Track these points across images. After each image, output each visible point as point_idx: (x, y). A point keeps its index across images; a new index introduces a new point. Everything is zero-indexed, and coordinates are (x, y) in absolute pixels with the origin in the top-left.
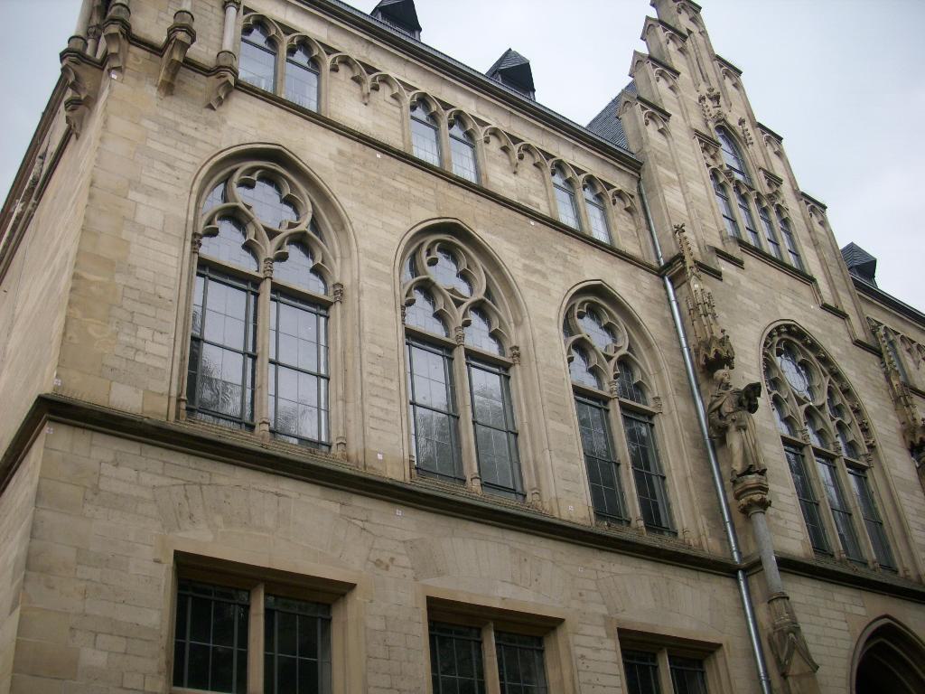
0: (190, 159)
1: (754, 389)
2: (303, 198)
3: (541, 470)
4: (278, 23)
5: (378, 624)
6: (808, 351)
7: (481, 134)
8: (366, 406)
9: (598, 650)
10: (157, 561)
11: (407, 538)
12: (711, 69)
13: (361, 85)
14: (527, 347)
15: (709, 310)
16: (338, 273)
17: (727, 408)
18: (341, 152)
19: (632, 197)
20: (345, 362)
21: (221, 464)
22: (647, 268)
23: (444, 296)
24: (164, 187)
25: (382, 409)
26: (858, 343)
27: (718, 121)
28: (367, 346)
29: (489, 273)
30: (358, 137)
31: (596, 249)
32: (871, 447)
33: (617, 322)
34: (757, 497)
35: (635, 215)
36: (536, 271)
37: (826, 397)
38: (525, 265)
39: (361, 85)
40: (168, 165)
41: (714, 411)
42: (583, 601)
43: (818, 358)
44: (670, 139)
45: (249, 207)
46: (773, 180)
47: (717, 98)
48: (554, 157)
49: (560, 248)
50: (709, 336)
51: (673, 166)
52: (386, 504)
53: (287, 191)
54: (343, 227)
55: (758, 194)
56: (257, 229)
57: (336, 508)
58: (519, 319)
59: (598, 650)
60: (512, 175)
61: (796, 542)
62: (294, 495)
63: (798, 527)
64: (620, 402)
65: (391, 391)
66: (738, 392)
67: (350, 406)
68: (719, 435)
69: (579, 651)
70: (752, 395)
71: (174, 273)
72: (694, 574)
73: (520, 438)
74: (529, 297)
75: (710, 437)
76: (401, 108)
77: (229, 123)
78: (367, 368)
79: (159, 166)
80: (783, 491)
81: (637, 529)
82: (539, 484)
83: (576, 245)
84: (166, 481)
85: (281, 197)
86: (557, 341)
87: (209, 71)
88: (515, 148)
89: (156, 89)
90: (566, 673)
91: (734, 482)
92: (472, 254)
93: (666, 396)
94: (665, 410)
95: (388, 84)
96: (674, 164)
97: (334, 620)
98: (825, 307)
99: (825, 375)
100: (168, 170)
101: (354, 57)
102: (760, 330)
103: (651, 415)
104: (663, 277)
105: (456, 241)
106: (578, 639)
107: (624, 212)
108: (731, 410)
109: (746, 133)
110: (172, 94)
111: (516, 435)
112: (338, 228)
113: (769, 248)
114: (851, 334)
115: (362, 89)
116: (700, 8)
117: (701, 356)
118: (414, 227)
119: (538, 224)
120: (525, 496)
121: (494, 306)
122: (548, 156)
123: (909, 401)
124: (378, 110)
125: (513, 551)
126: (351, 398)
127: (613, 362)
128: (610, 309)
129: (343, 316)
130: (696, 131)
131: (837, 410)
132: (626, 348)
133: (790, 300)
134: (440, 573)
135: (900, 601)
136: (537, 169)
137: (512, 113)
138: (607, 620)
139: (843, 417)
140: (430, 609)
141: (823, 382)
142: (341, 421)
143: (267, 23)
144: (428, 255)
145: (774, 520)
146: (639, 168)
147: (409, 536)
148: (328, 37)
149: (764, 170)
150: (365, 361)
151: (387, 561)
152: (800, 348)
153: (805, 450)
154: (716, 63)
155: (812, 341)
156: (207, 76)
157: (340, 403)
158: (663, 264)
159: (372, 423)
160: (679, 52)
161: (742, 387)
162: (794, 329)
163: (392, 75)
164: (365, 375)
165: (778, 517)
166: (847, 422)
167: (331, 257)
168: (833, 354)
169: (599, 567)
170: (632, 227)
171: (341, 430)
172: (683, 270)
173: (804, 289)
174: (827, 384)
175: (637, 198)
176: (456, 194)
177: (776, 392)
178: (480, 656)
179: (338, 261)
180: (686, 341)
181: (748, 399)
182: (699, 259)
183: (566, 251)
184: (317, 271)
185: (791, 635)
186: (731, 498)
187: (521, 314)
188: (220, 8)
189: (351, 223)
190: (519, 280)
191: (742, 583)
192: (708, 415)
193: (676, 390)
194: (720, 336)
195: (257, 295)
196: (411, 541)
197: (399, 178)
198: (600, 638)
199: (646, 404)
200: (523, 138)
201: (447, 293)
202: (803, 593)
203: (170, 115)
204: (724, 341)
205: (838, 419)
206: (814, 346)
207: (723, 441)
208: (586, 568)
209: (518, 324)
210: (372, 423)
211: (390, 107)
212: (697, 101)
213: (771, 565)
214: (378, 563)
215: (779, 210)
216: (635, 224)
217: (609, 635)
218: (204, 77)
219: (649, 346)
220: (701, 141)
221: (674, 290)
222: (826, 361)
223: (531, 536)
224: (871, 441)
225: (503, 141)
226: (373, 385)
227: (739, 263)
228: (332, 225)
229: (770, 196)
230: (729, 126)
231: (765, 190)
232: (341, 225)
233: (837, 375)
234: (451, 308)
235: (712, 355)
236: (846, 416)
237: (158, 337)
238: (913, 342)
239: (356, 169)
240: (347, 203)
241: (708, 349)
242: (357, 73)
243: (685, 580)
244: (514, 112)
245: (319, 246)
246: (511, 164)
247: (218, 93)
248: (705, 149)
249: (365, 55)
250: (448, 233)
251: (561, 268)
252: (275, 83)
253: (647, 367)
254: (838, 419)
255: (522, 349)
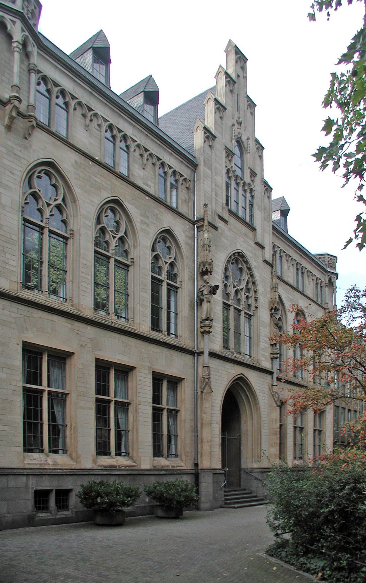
0: (20, 169)
1: (217, 287)
2: (60, 185)
3: (135, 311)
4: (52, 80)
5: (81, 366)
6: (244, 263)
7: (133, 147)
8: (80, 286)
9: (145, 378)
10: (18, 344)
11: (91, 337)
12: (243, 104)
13: (85, 119)
14: (137, 259)
15: (208, 249)
16: (71, 225)
17: (205, 292)
18: (76, 162)
19: (190, 181)
20: (73, 266)
21: (35, 309)
22: (189, 220)
23: (109, 233)
24: (11, 185)
25: (85, 287)
26: (265, 261)
27: (238, 138)
28: (81, 260)
29: (127, 222)
30: (84, 153)
31: (170, 211)
32: (256, 307)
33: (172, 246)
34: (207, 330)
35: (189, 191)
36: (145, 223)
37: (245, 284)
38: (141, 220)
39: (85, 119)
40: (11, 172)
41: (200, 292)
42: (143, 361)
43: (247, 267)
44: (213, 151)
45: (40, 191)
46: (253, 174)
47: (240, 124)
48: (161, 160)
49: (156, 211)
50: (206, 260)
51: (210, 167)
52: (85, 324)
53: (54, 182)
54: (75, 201)
55: (245, 182)
56: (43, 202)
57: (69, 326)
58: (136, 245)
59: (145, 378)
60: (142, 170)
61: (217, 347)
62: (57, 321)
63: (220, 340)
64: (167, 282)
65: (89, 279)
66: (210, 286)
67: (74, 284)
68: (200, 302)
69: (139, 378)
70: (215, 289)
71: (16, 228)
72: (180, 353)
73: (129, 297)
74: (140, 235)
75: (197, 301)
76: (101, 132)
77: (33, 147)
78: (81, 270)
79: (8, 173)
80: (218, 327)
81: (164, 334)
82: (134, 317)
83: (162, 209)
84: (19, 316)
85: (51, 183)
86: (148, 257)
87: (25, 116)
88: (146, 155)
89: (4, 128)
90: (135, 385)
91: (201, 322)
92: (121, 213)
93: (184, 281)
94: (183, 287)
95: (97, 117)
96: (211, 165)
97: (67, 363)
98: (257, 244)
99: (248, 274)
100: (11, 175)
101: (84, 102)
102: (226, 255)
103: (177, 288)
104: (194, 225)
105: (117, 207)
106: (140, 374)
107: (185, 189)
108: (206, 293)
109: (248, 146)
110: (10, 131)
111: (128, 295)
112: (72, 201)
113: (240, 214)
114: (263, 256)
115: (85, 121)
116: (247, 60)
117: (201, 268)
118: (102, 202)
119: (149, 198)
120: (128, 320)
121: (127, 239)
122: (159, 159)
123: (276, 290)
124: (91, 134)
125: (123, 342)
126: (75, 282)
127: (168, 264)
128: (170, 239)
129: (73, 245)
130: (226, 147)
131: (248, 290)
132: (173, 258)
133: (242, 240)
134: (100, 350)
135: (248, 369)
136: (153, 166)
137: (147, 135)
138: (150, 368)
139: (249, 294)
140: (96, 361)
141: (245, 277)
142: (71, 291)
143: (47, 80)
144: (105, 213)
145: (212, 337)
146: (196, 167)
147: (91, 336)
148: (73, 89)
149: (250, 169)
150: (80, 266)
151: (84, 345)
152: (241, 262)
153: (231, 307)
154: (246, 99)
155: (246, 260)
156: (23, 118)
157: (71, 283)
158: (196, 219)
159: (82, 293)
160: (230, 92)
161: (213, 285)
162: (241, 254)
163: (99, 113)
164: (80, 273)
165: (213, 336)
166: (250, 296)
167: (70, 216)
168: (253, 266)
169: (149, 349)
170: (187, 197)
171: (71, 294)
172: (203, 225)
173: (250, 234)
174: (247, 279)
175: (192, 181)
176: (119, 183)
177: (226, 282)
178: (109, 377)
179: (72, 218)
180: (197, 257)
181: (214, 290)
182: (210, 221)
183: (158, 212)
184: (64, 222)
185: (207, 380)
186: (199, 327)
187: (137, 244)
188: (27, 71)
189: (78, 201)
190: (138, 228)
191: (196, 358)
192: (198, 293)
193: (189, 279)
194: (210, 261)
195: (42, 234)
196: (92, 338)
197: (98, 176)
198: (146, 374)
199: (176, 283)
200: (150, 149)
201: (110, 232)
202: (215, 364)
203: (10, 143)
204: (210, 264)
205: (247, 294)
206: (246, 262)
207: (201, 304)
208: (145, 349)
209: (135, 247)
210: (82, 293)
211: (96, 131)
212: (231, 125)
213: (206, 354)
214: (82, 346)
215: (251, 190)
216: (188, 195)
217: (149, 373)
218: (23, 119)
219: (182, 258)
220: (226, 152)
221: (197, 232)
222: (249, 269)
223: (129, 337)
224: (257, 306)
225: (141, 151)
226: (83, 277)
227: (225, 221)
228: (70, 199)
229: (249, 184)
230: (242, 141)
231: (247, 180)
232: (74, 201)
233: (252, 276)
234: (111, 239)
235: (204, 270)
236: (251, 293)
237: (13, 258)
238: (290, 257)
239: (81, 171)
240: (77, 191)
241: (204, 266)
242: (84, 112)
243: (177, 355)
244: (149, 135)
245: (65, 210)
246: (143, 164)
247: (29, 132)
248: (227, 156)
249: (88, 100)
250: (114, 203)
251: (155, 221)
252: (49, 120)
253: (180, 267)
254: (247, 294)
255: (135, 259)
